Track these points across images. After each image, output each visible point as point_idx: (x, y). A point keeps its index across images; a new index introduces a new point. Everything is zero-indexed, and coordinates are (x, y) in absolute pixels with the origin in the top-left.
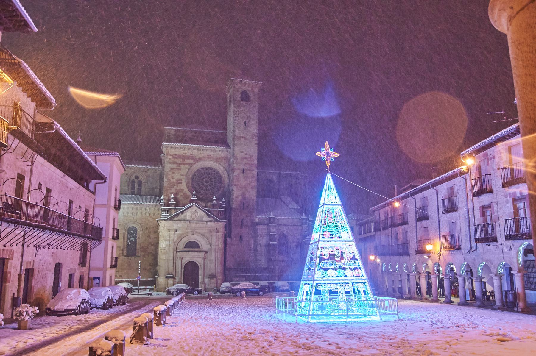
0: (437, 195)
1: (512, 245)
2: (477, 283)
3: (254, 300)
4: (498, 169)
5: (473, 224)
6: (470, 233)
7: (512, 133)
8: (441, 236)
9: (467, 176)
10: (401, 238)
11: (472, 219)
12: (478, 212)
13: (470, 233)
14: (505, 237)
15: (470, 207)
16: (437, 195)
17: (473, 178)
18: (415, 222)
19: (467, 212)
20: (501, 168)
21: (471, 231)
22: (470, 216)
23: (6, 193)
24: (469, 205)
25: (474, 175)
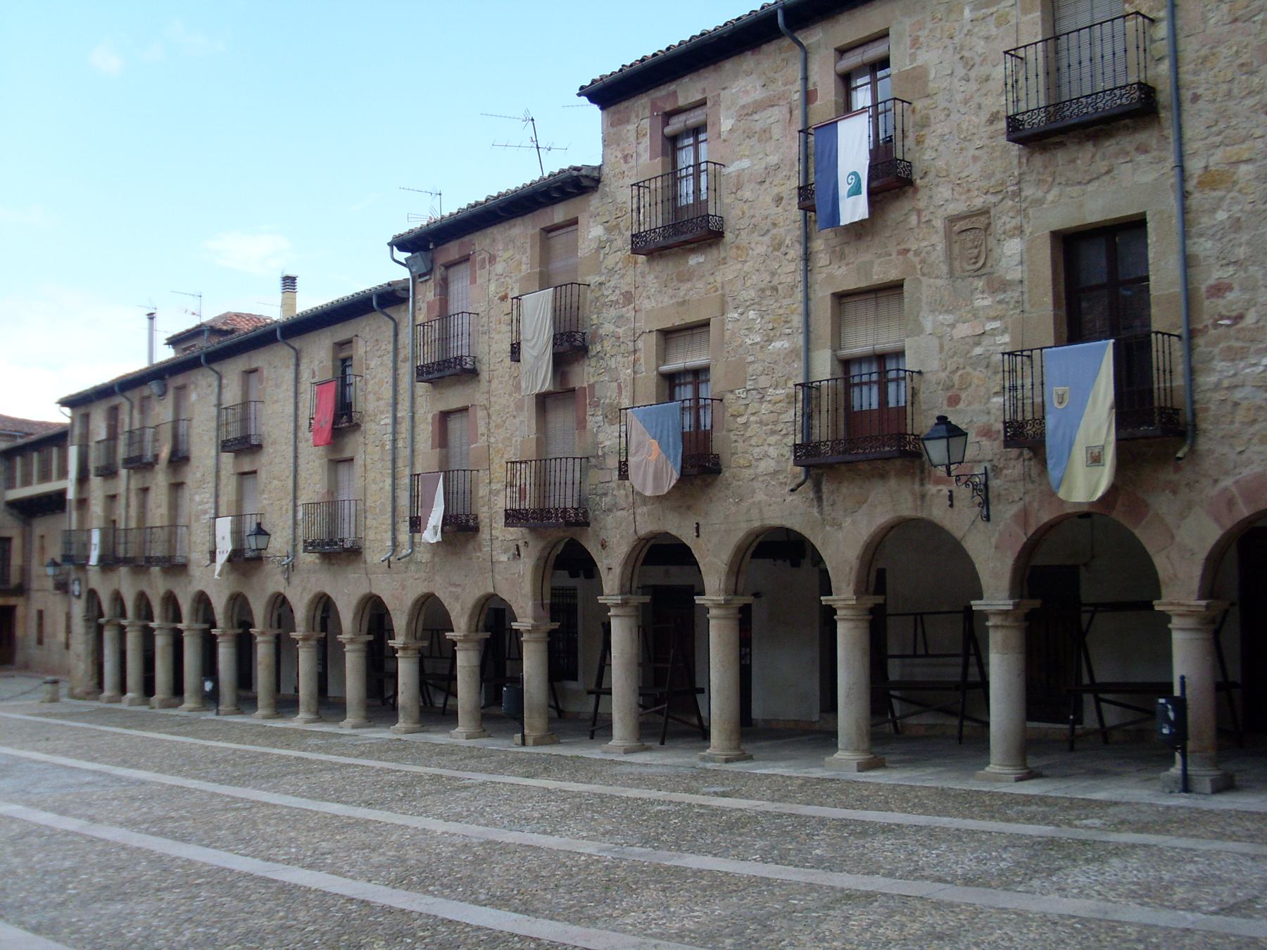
0: (940, 613)
1: (521, 543)
3: (661, 256)
4: (504, 298)
5: (407, 472)
6: (394, 499)
7: (558, 189)
8: (300, 502)
9: (405, 317)
10: (159, 506)
11: (404, 452)
12: (426, 431)
13: (394, 499)
14: (506, 519)
15: (404, 412)
16: (940, 613)
17: (421, 318)
18: (213, 453)
19: (390, 429)
20: (511, 295)
21: (399, 493)
22: (400, 444)
23: (942, 420)
24: (399, 407)
25: (425, 310)
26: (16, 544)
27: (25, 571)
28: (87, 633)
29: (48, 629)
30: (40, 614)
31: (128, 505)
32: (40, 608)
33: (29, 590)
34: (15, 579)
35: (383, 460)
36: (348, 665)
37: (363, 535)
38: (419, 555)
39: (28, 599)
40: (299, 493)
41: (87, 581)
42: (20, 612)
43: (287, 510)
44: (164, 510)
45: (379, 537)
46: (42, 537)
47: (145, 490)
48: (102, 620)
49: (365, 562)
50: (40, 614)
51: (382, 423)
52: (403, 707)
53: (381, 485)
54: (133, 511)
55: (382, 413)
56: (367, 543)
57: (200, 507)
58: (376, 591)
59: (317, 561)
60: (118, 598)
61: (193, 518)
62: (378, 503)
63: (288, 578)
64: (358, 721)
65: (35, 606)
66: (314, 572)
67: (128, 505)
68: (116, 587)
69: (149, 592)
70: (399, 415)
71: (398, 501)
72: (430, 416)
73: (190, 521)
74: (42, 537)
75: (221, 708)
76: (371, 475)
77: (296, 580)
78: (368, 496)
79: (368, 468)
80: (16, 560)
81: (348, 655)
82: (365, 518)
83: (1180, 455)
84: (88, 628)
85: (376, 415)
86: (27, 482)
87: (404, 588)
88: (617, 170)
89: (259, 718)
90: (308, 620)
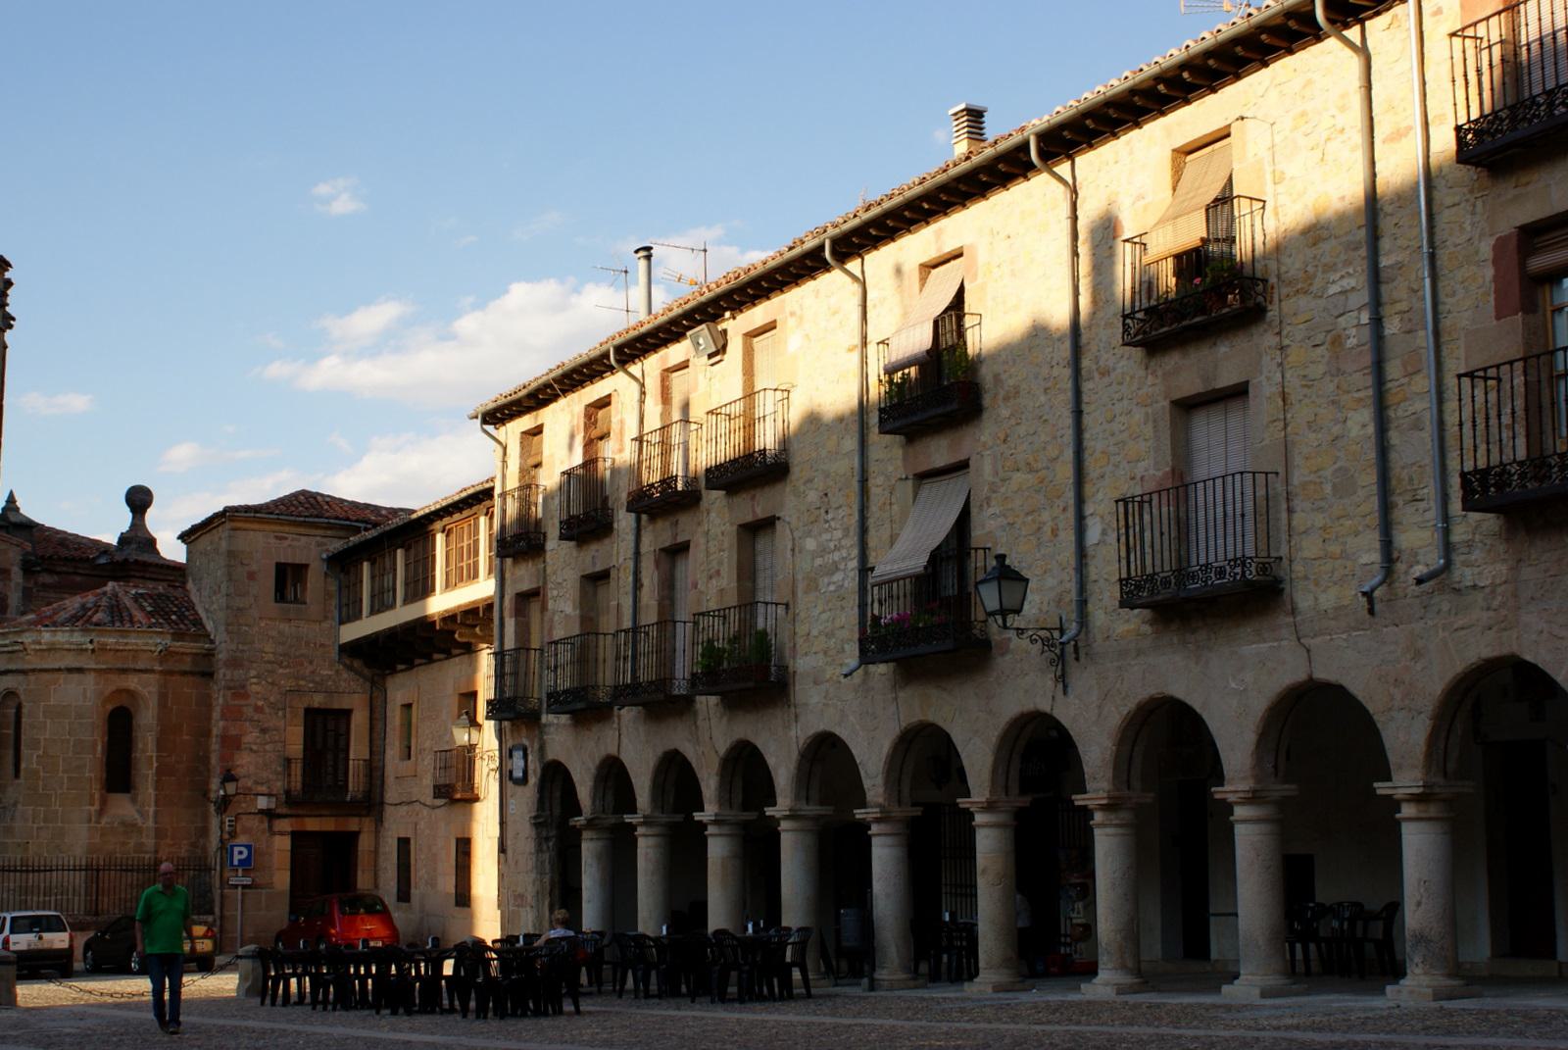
2: (651, 841)
26: (359, 720)
27: (374, 770)
28: (539, 850)
29: (419, 872)
30: (404, 844)
31: (637, 585)
32: (403, 835)
33: (382, 803)
34: (355, 784)
35: (1339, 372)
36: (1239, 852)
37: (1284, 551)
38: (1468, 571)
39: (379, 821)
40: (1088, 489)
41: (542, 749)
42: (365, 843)
43: (1055, 532)
44: (728, 580)
45: (1335, 548)
46: (408, 706)
47: (678, 551)
48: (579, 821)
49: (1294, 612)
50: (404, 844)
51: (1334, 289)
52: (1420, 939)
53: (1336, 430)
54: (649, 597)
55: (1330, 268)
56: (1298, 567)
57: (819, 561)
58: (1325, 672)
59: (1147, 629)
60: (613, 774)
61: (801, 587)
62: (1328, 473)
63: (1063, 676)
64: (1274, 981)
65: (396, 823)
66: (1139, 653)
67: (637, 585)
68: (613, 751)
69: (690, 752)
70: (1384, 262)
71: (1393, 456)
72: (1486, 249)
73: (794, 593)
74: (408, 706)
75: (882, 974)
76: (1301, 414)
77: (1083, 679)
78: (1298, 460)
79: (1293, 398)
80: (358, 750)
81: (1240, 830)
82: (1290, 511)
83: (380, 944)
84: (541, 841)
85: (1310, 278)
86: (381, 604)
87: (1418, 655)
88: (713, 571)
89: (279, 1009)
90: (1116, 767)
